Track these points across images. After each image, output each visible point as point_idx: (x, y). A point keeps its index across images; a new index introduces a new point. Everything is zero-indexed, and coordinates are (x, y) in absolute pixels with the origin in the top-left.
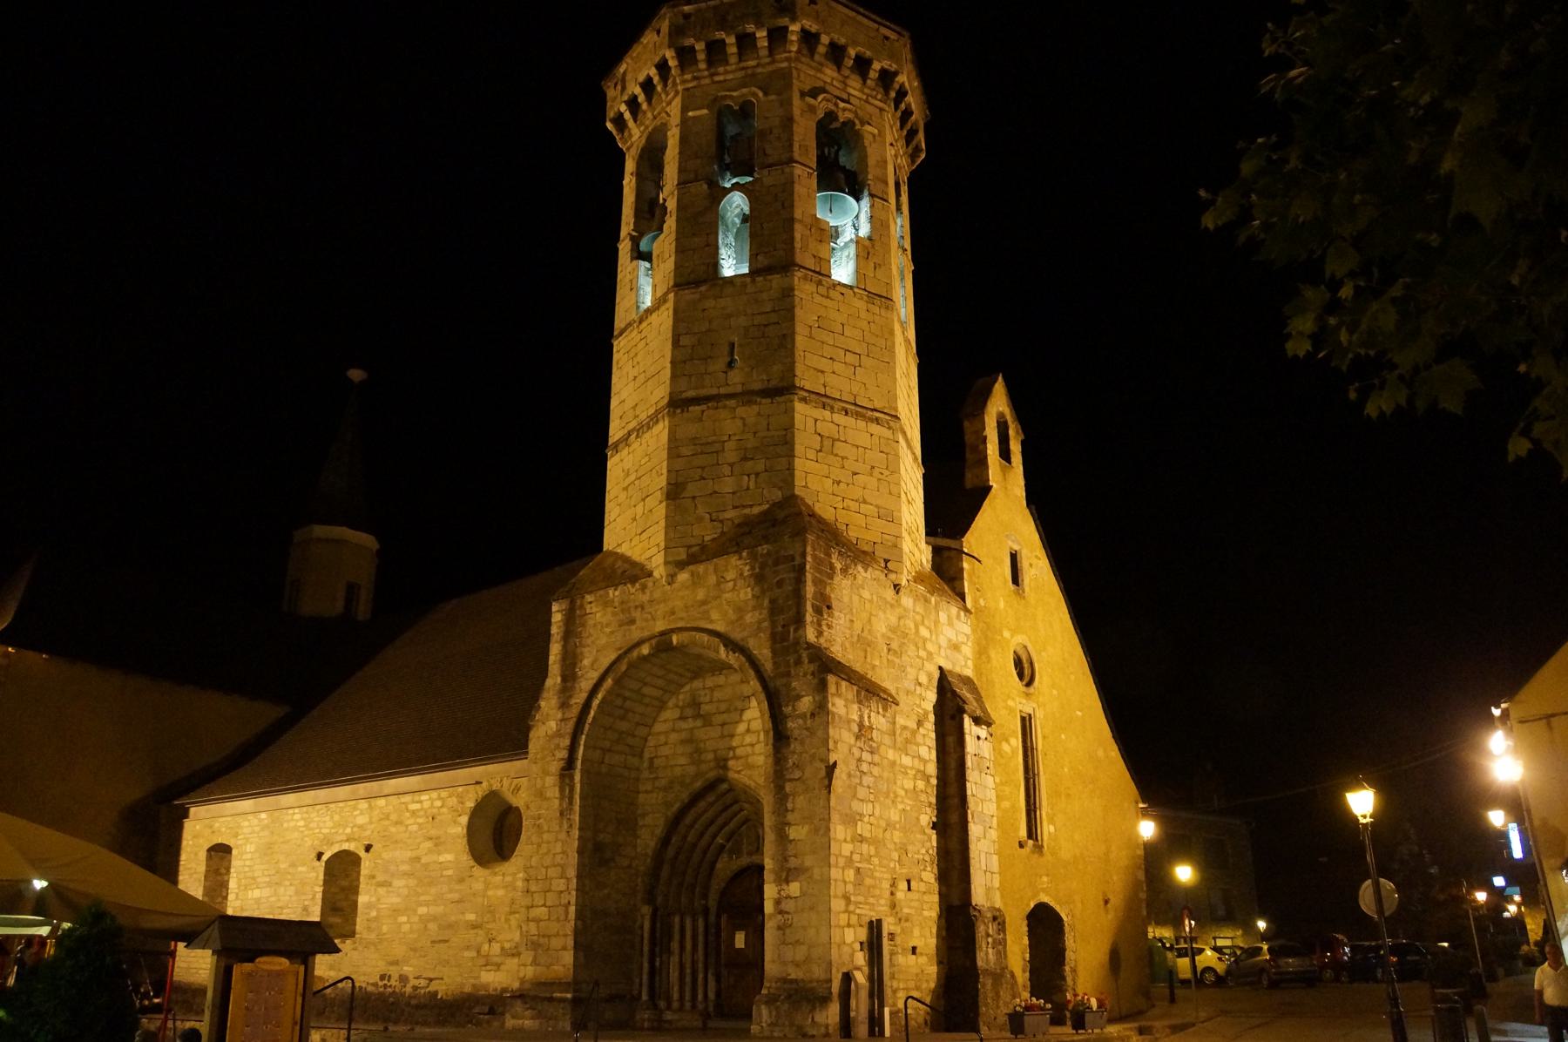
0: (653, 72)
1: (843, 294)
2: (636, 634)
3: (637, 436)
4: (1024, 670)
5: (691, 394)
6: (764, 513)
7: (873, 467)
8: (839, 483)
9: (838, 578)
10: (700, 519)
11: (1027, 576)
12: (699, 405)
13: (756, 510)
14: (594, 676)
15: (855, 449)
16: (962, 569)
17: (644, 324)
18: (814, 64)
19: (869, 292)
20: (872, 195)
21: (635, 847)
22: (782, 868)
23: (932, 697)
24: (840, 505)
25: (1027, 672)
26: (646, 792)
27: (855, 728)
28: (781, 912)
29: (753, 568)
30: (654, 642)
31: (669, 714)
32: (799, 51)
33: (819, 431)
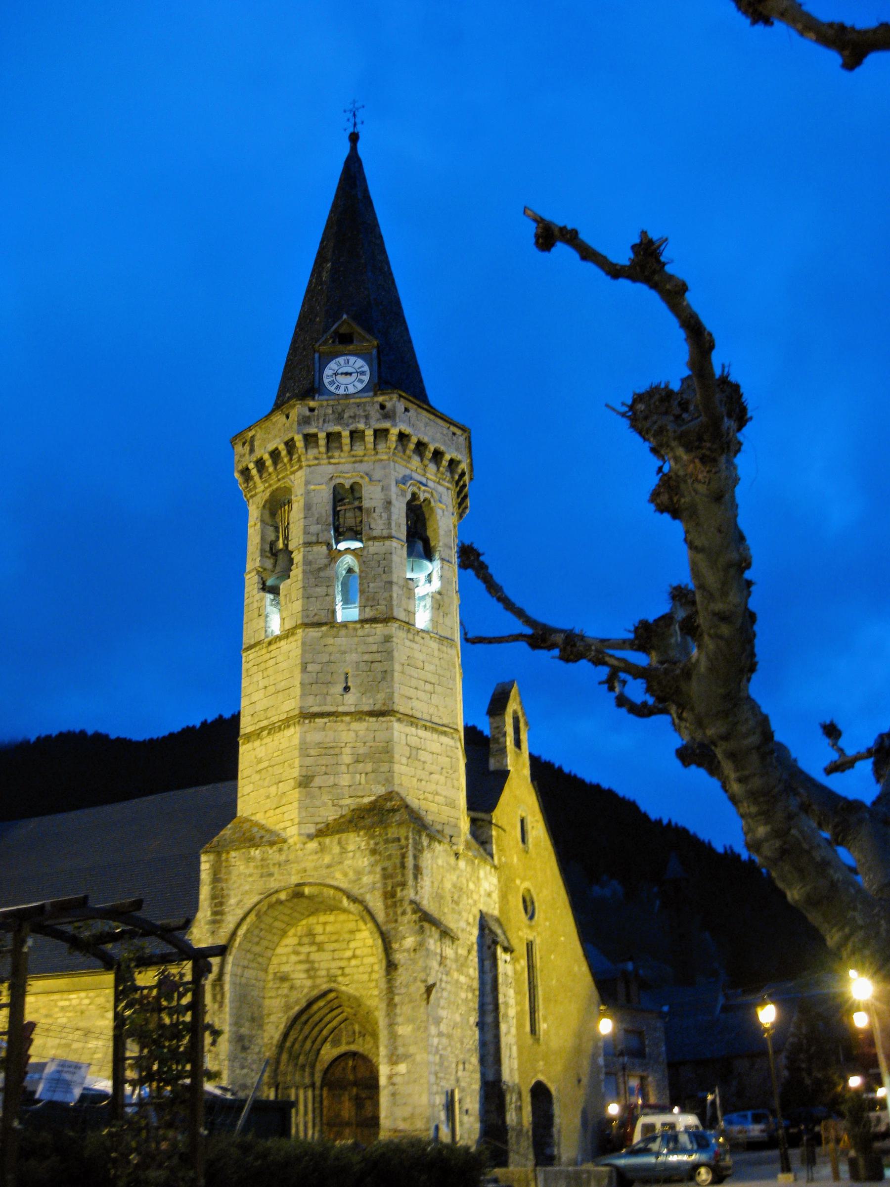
0: (282, 447)
1: (423, 638)
2: (273, 884)
3: (269, 734)
4: (529, 906)
5: (316, 709)
6: (374, 804)
7: (442, 768)
8: (421, 780)
9: (426, 852)
10: (324, 804)
11: (532, 835)
12: (323, 718)
13: (366, 800)
14: (240, 913)
15: (431, 755)
16: (491, 836)
17: (273, 647)
18: (405, 457)
19: (441, 636)
20: (442, 559)
21: (262, 1038)
22: (392, 1054)
23: (476, 932)
24: (421, 797)
25: (530, 908)
26: (271, 997)
27: (438, 958)
28: (393, 1084)
29: (368, 844)
30: (290, 891)
31: (290, 940)
32: (396, 448)
33: (409, 743)
